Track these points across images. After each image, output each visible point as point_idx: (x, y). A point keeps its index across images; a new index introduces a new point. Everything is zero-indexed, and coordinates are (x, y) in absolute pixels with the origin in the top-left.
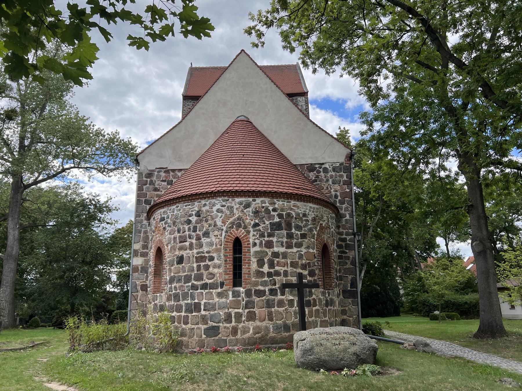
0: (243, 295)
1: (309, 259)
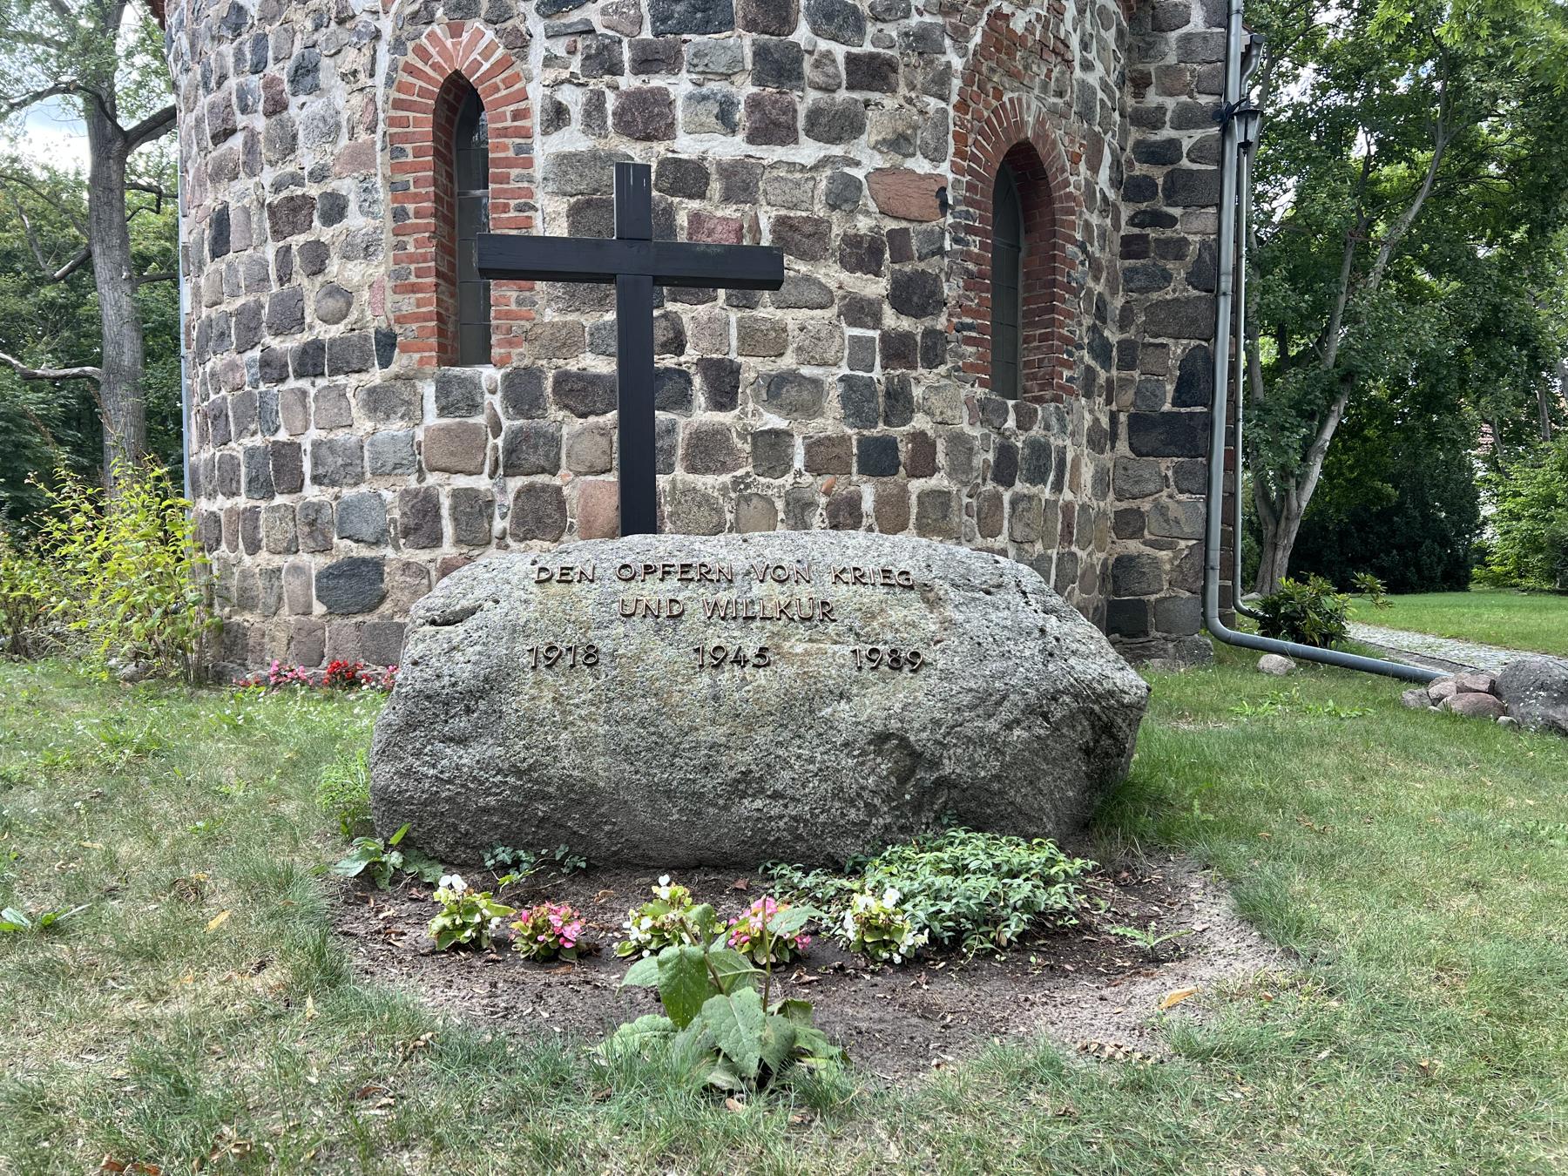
0: (496, 401)
1: (902, 211)
